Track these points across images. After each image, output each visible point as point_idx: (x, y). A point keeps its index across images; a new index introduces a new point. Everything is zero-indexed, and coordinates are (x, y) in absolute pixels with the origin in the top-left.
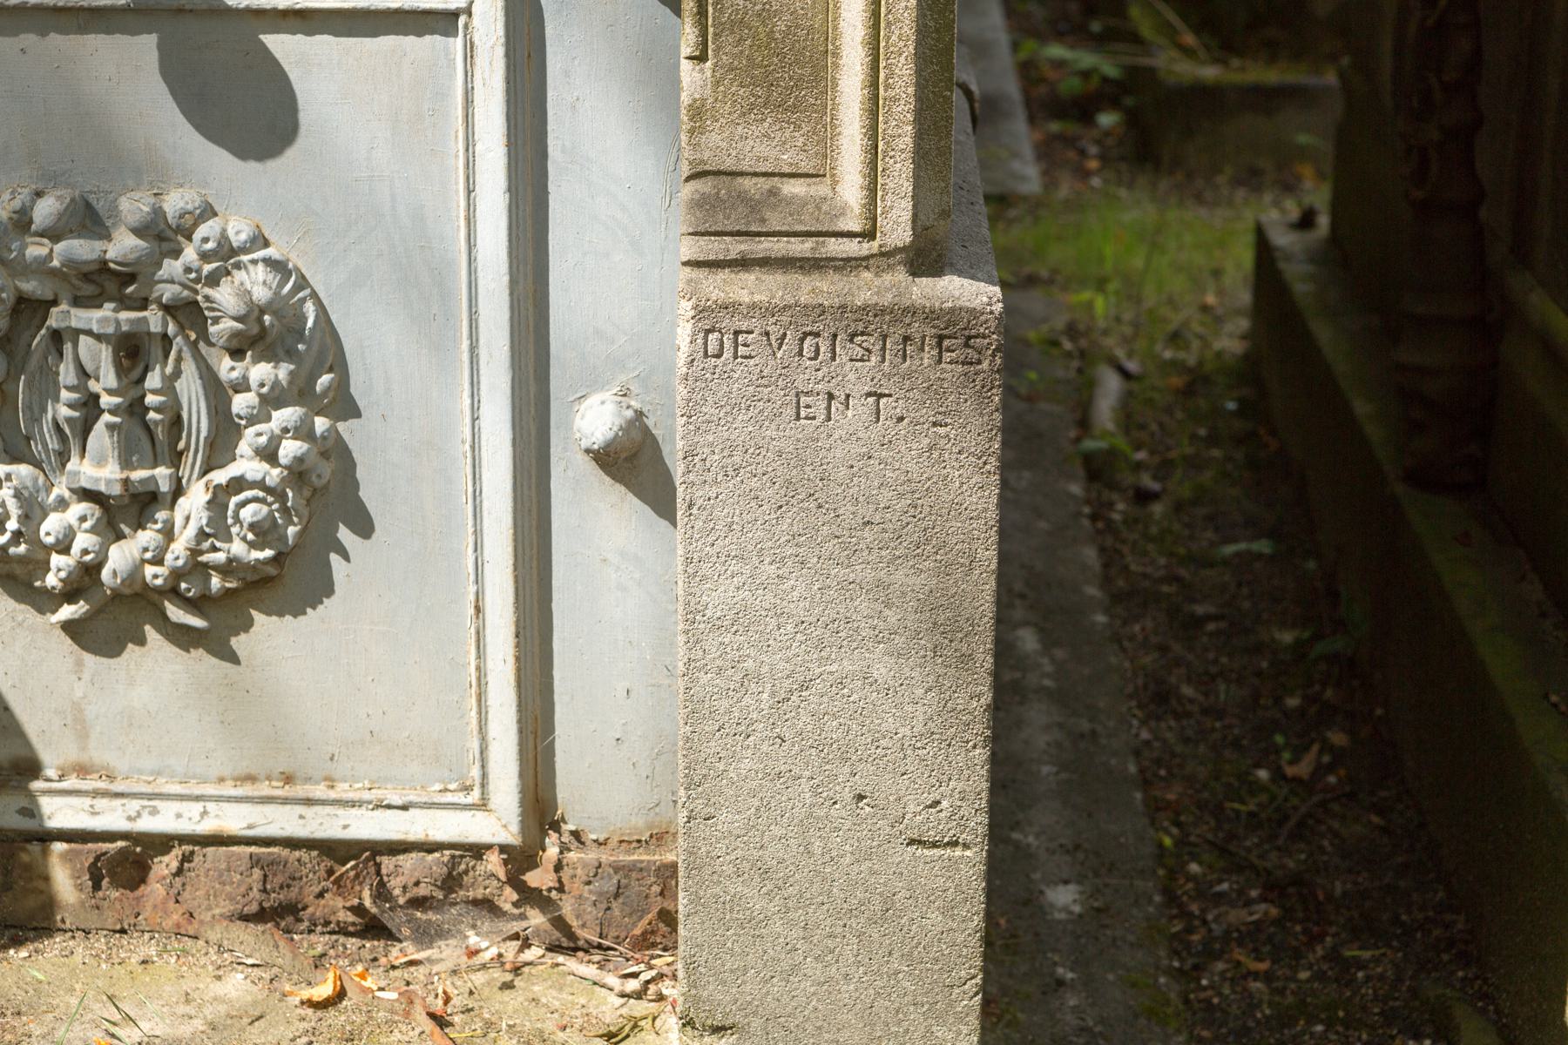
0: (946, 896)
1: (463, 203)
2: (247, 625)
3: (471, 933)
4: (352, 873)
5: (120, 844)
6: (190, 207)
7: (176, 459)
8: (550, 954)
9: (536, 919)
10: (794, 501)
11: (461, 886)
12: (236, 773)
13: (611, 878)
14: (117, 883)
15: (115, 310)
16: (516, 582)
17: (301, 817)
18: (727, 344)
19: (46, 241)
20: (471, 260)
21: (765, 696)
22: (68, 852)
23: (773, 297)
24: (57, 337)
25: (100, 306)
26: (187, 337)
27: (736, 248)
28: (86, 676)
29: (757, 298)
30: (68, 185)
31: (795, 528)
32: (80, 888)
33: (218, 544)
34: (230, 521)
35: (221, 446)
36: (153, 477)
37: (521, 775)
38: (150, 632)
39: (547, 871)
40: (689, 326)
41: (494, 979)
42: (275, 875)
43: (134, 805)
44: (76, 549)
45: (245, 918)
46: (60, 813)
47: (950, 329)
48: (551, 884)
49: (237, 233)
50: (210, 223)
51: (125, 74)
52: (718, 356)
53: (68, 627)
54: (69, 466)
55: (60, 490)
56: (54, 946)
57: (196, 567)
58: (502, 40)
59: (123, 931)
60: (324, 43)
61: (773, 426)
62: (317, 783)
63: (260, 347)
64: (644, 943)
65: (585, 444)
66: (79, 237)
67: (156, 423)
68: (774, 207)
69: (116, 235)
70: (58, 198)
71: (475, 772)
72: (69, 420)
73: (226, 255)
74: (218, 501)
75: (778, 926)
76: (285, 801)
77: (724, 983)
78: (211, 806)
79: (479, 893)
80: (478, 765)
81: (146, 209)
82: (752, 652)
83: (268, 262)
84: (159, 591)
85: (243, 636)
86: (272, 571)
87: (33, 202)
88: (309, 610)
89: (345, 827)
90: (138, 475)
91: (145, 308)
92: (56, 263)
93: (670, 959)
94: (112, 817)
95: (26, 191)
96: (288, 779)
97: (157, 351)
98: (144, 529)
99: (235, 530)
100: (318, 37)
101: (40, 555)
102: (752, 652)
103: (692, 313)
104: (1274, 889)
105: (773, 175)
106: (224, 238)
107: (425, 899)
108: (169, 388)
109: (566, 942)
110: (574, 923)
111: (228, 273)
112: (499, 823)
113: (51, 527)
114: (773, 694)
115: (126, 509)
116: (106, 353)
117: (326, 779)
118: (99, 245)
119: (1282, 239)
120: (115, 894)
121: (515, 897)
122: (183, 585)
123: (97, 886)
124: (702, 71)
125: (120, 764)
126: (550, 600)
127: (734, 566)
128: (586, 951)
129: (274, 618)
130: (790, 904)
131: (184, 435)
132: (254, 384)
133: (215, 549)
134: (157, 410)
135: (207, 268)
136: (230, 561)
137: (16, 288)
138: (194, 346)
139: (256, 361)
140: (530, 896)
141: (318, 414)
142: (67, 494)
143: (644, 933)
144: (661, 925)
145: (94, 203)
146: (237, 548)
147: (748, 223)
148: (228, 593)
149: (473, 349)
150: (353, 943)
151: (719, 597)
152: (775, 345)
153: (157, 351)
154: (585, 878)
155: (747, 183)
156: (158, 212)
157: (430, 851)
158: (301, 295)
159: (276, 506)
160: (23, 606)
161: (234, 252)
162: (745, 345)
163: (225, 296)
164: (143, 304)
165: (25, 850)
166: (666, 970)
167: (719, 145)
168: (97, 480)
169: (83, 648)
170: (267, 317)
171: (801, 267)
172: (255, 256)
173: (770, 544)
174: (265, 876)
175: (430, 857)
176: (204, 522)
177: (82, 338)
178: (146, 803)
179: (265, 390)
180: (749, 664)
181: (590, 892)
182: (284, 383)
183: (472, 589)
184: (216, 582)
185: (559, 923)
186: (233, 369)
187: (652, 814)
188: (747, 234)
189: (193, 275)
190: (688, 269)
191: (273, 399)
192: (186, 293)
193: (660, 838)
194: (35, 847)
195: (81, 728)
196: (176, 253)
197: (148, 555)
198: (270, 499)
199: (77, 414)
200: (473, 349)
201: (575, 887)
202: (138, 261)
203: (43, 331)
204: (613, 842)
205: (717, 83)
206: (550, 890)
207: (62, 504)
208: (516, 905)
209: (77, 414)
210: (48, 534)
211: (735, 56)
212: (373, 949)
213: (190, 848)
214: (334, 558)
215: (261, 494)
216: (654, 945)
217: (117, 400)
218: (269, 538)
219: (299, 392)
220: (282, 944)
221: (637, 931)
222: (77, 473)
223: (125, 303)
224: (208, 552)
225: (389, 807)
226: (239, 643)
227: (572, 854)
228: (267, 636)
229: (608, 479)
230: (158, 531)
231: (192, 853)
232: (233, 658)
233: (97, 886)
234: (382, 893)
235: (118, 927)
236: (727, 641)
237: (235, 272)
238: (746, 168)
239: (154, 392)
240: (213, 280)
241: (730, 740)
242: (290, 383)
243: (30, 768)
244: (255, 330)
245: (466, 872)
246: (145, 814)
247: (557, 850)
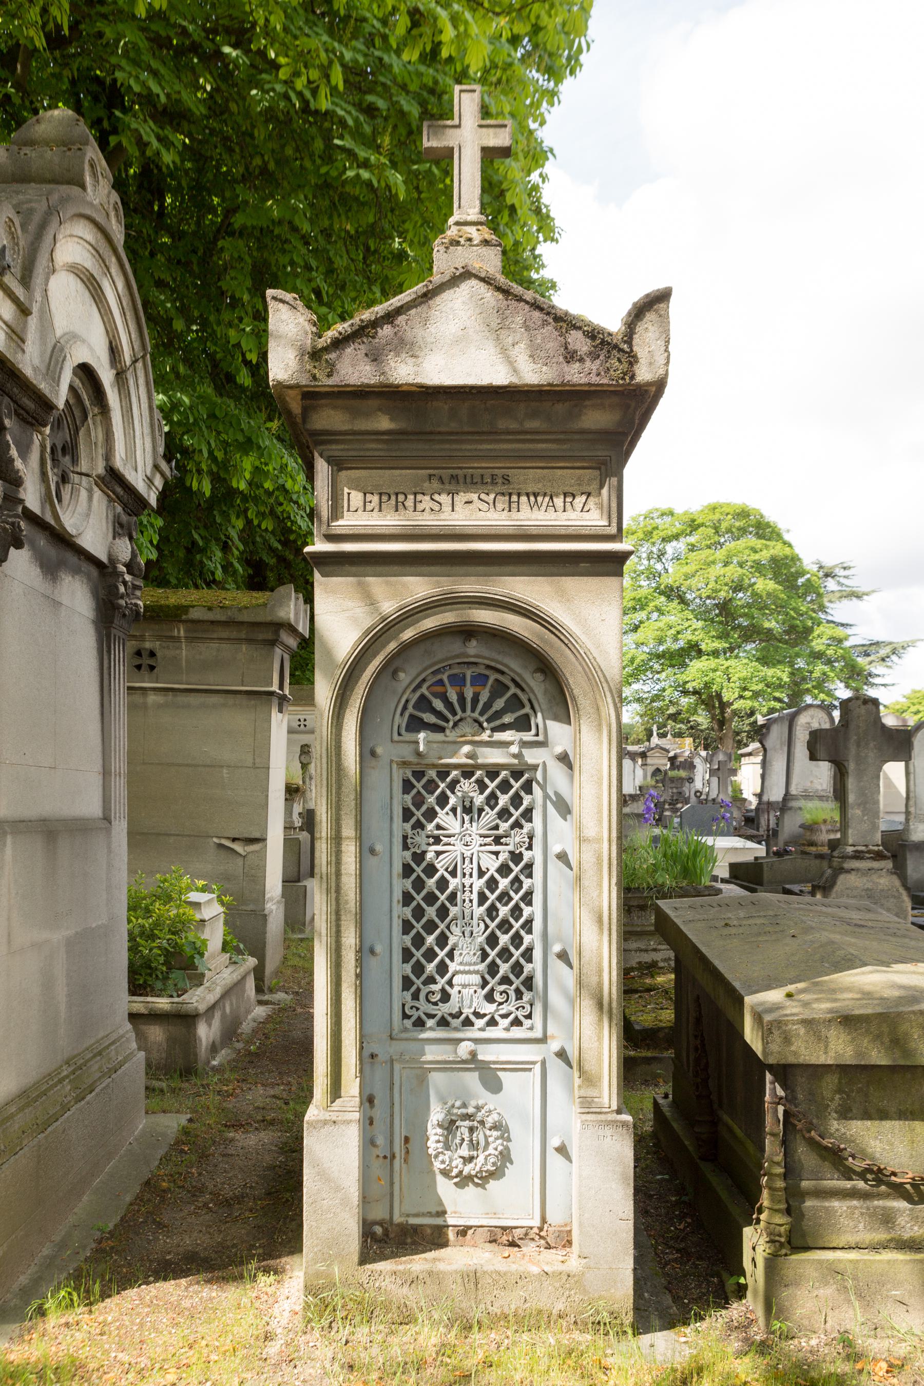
0: (628, 1227)
47: (624, 1124)
53: (456, 1184)
56: (449, 1249)
57: (481, 1171)
64: (564, 1246)
74: (486, 1159)
94: (461, 1222)
104: (678, 1251)
109: (549, 1247)
112: (536, 1223)
113: (454, 1164)
119: (661, 1101)
140: (541, 1237)
191: (497, 1139)
219: (502, 1137)
228: (492, 1184)
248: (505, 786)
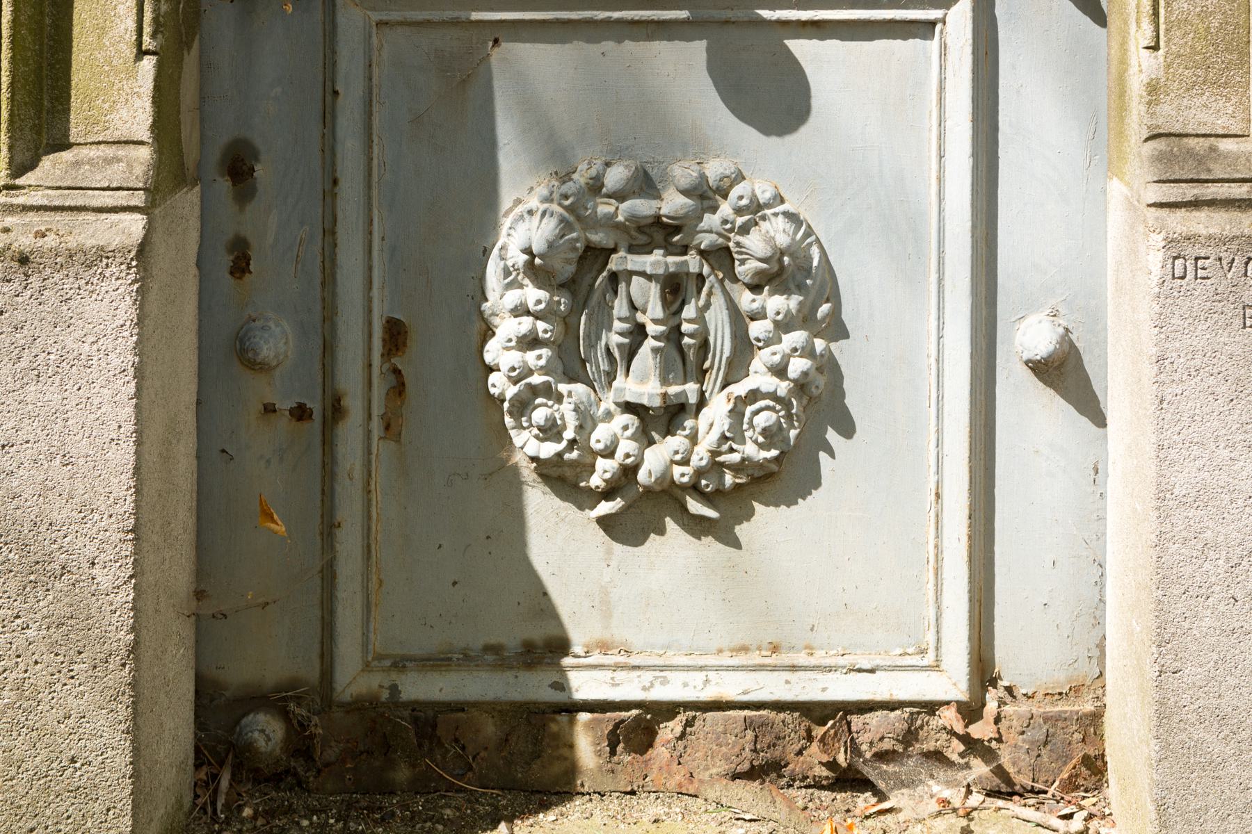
1: (934, 166)
2: (749, 514)
3: (931, 782)
4: (832, 732)
5: (634, 712)
6: (728, 172)
7: (701, 375)
8: (989, 800)
9: (980, 768)
10: (1242, 395)
11: (917, 740)
12: (732, 645)
13: (1040, 727)
14: (630, 749)
15: (665, 255)
16: (971, 472)
17: (787, 682)
18: (1190, 268)
19: (613, 201)
20: (940, 211)
21: (1221, 562)
22: (591, 721)
23: (1223, 230)
24: (614, 278)
25: (650, 252)
26: (716, 276)
27: (1190, 192)
28: (614, 563)
29: (1211, 231)
30: (630, 157)
31: (1244, 418)
32: (599, 754)
33: (735, 446)
34: (745, 426)
35: (737, 367)
36: (684, 392)
37: (970, 639)
38: (670, 523)
39: (988, 723)
40: (1160, 255)
41: (952, 825)
42: (764, 735)
43: (648, 676)
44: (619, 454)
45: (735, 776)
46: (585, 685)
48: (992, 735)
49: (763, 192)
50: (742, 184)
51: (681, 71)
52: (1183, 278)
53: (604, 522)
54: (615, 384)
55: (608, 403)
56: (576, 807)
57: (715, 467)
58: (970, 41)
59: (633, 793)
60: (833, 47)
61: (1226, 334)
62: (799, 651)
63: (776, 282)
64: (1071, 785)
65: (1026, 356)
66: (640, 197)
67: (690, 346)
68: (1216, 160)
69: (664, 195)
70: (626, 167)
71: (931, 637)
72: (620, 346)
73: (755, 209)
75: (1233, 768)
76: (774, 668)
77: (1189, 822)
78: (712, 675)
79: (930, 746)
80: (933, 630)
81: (695, 174)
82: (1211, 524)
83: (787, 215)
84: (683, 487)
85: (745, 525)
86: (774, 467)
87: (605, 170)
88: (800, 501)
89: (824, 690)
90: (673, 390)
91: (685, 253)
92: (620, 218)
93: (1095, 800)
94: (630, 688)
95: (599, 162)
96: (775, 649)
97: (692, 288)
98: (674, 435)
99: (748, 434)
100: (828, 41)
101: (588, 460)
102: (1211, 524)
103: (1163, 243)
105: (1210, 136)
106: (754, 198)
107: (887, 752)
108: (700, 319)
109: (1004, 788)
110: (1011, 770)
111: (756, 224)
112: (951, 683)
113: (600, 436)
114: (1228, 560)
115: (666, 418)
116: (654, 290)
117: (807, 647)
118: (655, 204)
120: (627, 758)
121: (962, 748)
122: (704, 482)
123: (613, 753)
124: (1156, 57)
125: (635, 639)
126: (994, 487)
127: (1196, 451)
128: (1021, 796)
129: (772, 508)
130: (1243, 747)
131: (710, 356)
132: (770, 312)
133: (732, 450)
134: (691, 336)
135: (740, 221)
136: (743, 459)
137: (587, 240)
138: (721, 282)
139: (772, 293)
141: (815, 336)
142: (613, 407)
143: (1070, 777)
144: (1083, 769)
145: (650, 171)
146: (750, 450)
147: (1198, 173)
148: (737, 487)
149: (940, 280)
150: (826, 795)
151: (1183, 479)
152: (1226, 267)
153: (692, 288)
154: (1019, 729)
155: (1192, 142)
156: (703, 177)
157: (893, 710)
158: (809, 240)
159: (782, 413)
160: (567, 504)
161: (760, 207)
162: (1203, 269)
163: (755, 243)
164: (684, 250)
165: (554, 720)
166: (1094, 810)
167: (1170, 115)
168: (641, 395)
169: (613, 539)
170: (786, 259)
171: (1239, 207)
172: (777, 210)
173: (1224, 431)
174: (756, 737)
175: (893, 715)
176: (726, 427)
177: (634, 278)
178: (658, 674)
179: (780, 317)
180: (1208, 534)
181: (1024, 741)
182: (794, 311)
183: (933, 479)
184: (729, 479)
185: (1000, 772)
186: (754, 301)
187: (1071, 669)
188: (1198, 181)
189: (729, 226)
190: (1153, 209)
191: (784, 325)
192: (721, 240)
193: (1076, 690)
194: (563, 718)
195: (605, 607)
196: (714, 209)
197: (678, 457)
198: (778, 407)
199: (626, 341)
200: (940, 280)
201: (1011, 737)
202: (686, 216)
203: (605, 274)
204: (1039, 696)
205: (1168, 66)
206: (990, 741)
207: (609, 416)
208: (962, 755)
209: (626, 341)
210: (598, 441)
211: (1181, 46)
212: (844, 800)
213: (693, 713)
214: (823, 455)
215: (771, 403)
216: (1077, 788)
217: (662, 328)
218: (776, 439)
219: (803, 319)
220: (779, 799)
221: (1065, 775)
222: (622, 390)
223: (670, 250)
224: (725, 453)
225: (860, 670)
226: (741, 530)
227: (1006, 708)
228: (766, 524)
229: (1041, 384)
230: (686, 437)
231: (694, 718)
232: (737, 544)
233: (613, 753)
234: (855, 749)
235: (629, 789)
236: (1190, 515)
237: (761, 223)
238: (1190, 131)
239: (689, 321)
240: (745, 230)
241: (1193, 602)
242: (799, 311)
243: (561, 646)
244: (776, 268)
245: (921, 727)
246: (657, 684)
247: (996, 704)
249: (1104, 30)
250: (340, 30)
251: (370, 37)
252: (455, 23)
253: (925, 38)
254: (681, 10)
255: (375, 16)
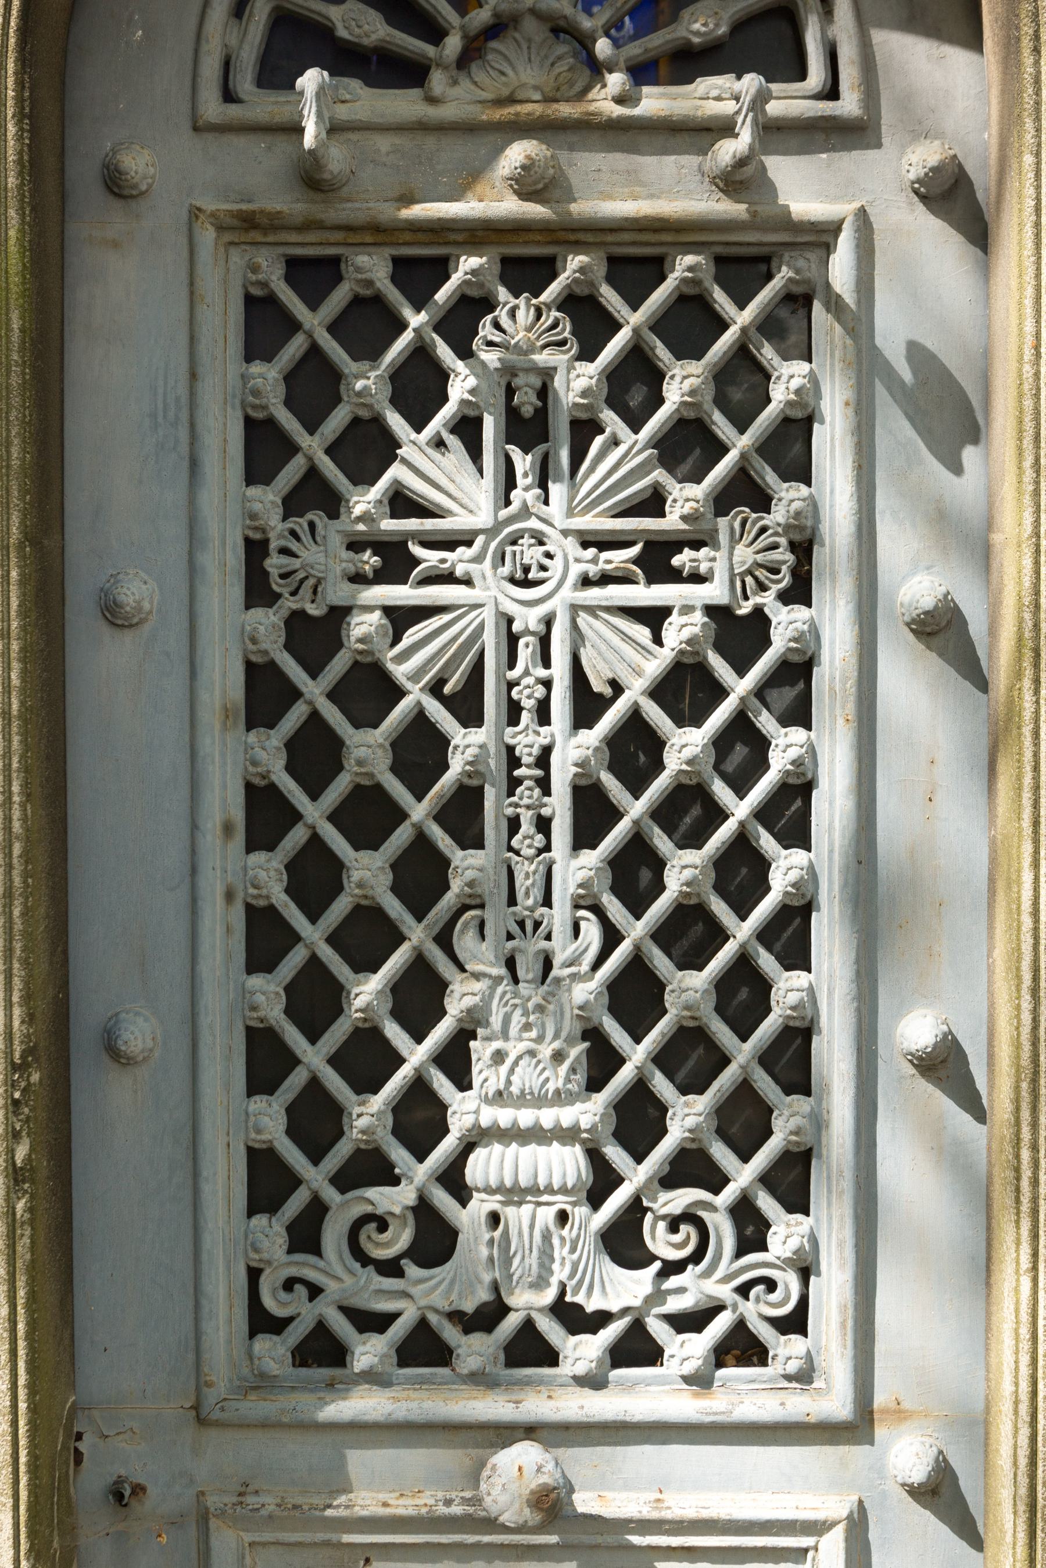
65: (900, 1480)
248: (690, 324)
249: (981, 1555)
250: (213, 1553)
251: (243, 1558)
252: (327, 1544)
253: (797, 1562)
254: (549, 1534)
255: (248, 1537)
